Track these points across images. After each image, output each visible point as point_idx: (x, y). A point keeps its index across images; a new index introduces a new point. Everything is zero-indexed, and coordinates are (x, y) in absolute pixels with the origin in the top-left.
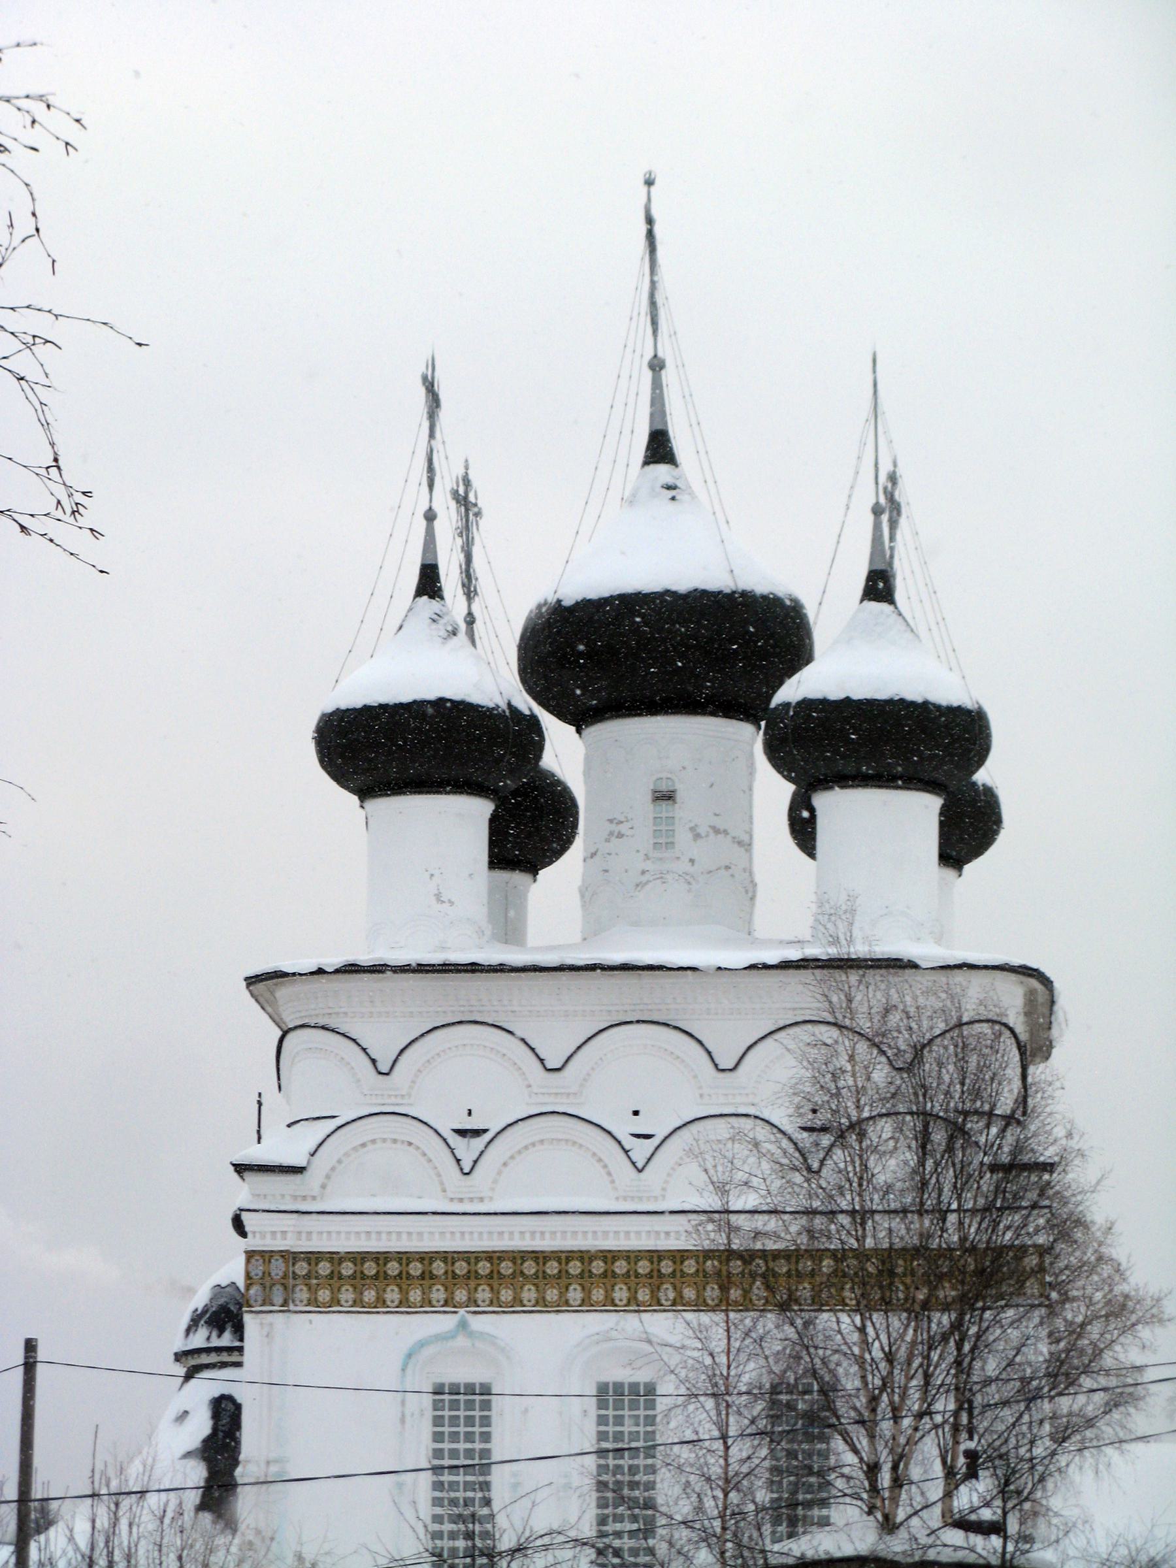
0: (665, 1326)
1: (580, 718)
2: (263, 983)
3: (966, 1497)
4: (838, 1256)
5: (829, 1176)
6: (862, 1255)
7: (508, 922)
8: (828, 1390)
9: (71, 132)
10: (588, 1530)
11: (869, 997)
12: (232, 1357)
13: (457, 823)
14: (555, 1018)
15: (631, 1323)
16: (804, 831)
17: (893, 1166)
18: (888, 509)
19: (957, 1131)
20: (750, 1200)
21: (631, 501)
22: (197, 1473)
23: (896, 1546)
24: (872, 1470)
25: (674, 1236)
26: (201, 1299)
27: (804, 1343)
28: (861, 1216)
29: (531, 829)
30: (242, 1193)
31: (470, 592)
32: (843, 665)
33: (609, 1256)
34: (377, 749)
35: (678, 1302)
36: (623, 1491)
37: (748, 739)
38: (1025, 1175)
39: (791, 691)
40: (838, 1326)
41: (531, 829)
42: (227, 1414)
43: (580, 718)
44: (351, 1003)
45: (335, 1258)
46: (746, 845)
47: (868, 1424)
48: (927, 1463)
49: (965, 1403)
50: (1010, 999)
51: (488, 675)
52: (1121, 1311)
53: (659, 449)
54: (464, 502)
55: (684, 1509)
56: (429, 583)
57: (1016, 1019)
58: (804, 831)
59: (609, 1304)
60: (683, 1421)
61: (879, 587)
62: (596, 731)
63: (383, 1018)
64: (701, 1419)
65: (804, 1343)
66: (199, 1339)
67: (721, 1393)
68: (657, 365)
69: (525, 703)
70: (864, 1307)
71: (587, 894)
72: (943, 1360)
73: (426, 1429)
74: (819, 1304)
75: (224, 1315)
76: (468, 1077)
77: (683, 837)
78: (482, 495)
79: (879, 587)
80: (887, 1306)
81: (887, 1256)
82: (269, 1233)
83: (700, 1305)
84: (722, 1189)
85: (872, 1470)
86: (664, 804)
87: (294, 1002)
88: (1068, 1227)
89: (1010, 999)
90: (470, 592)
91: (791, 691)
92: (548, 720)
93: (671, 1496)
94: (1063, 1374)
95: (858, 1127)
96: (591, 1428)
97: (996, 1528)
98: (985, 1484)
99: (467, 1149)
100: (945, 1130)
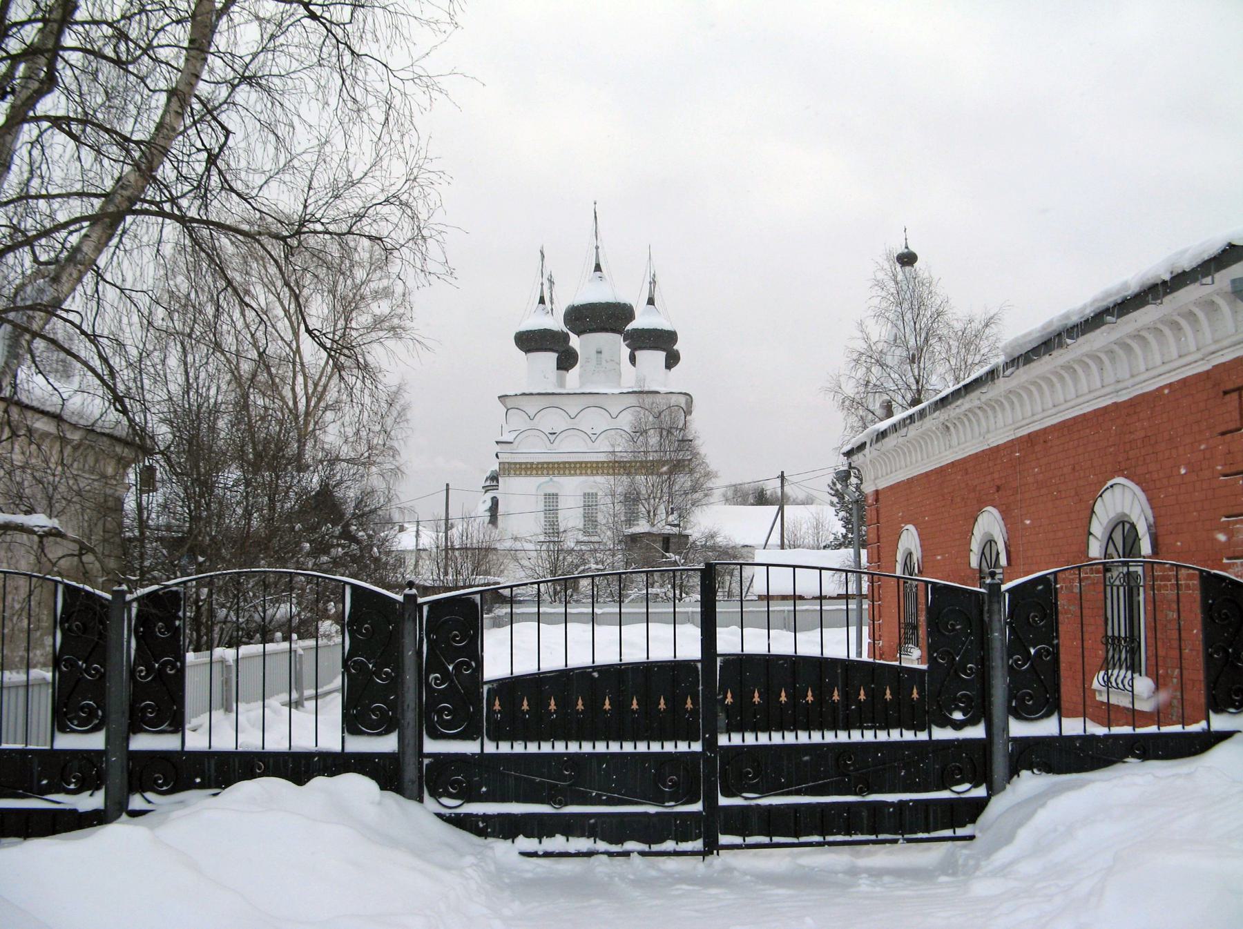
0: (600, 479)
1: (579, 333)
2: (502, 398)
3: (671, 518)
4: (641, 462)
6: (647, 462)
7: (561, 383)
9: (449, 180)
10: (581, 526)
11: (648, 400)
12: (496, 488)
13: (549, 359)
14: (573, 406)
15: (592, 478)
16: (633, 359)
17: (654, 439)
18: (653, 282)
19: (669, 432)
20: (620, 449)
23: (654, 530)
24: (649, 512)
25: (602, 458)
26: (488, 474)
27: (633, 482)
28: (646, 452)
29: (567, 360)
30: (498, 448)
31: (552, 303)
32: (642, 320)
33: (586, 463)
34: (530, 341)
35: (603, 474)
36: (590, 521)
37: (618, 338)
38: (685, 443)
39: (630, 327)
40: (640, 479)
42: (495, 502)
44: (526, 404)
45: (520, 464)
47: (647, 500)
49: (670, 495)
50: (682, 401)
51: (556, 323)
52: (708, 475)
53: (598, 268)
54: (551, 282)
55: (604, 522)
56: (542, 301)
57: (683, 405)
58: (633, 359)
59: (586, 474)
60: (605, 503)
61: (651, 301)
62: (583, 336)
63: (531, 406)
64: (609, 500)
65: (633, 482)
66: (488, 483)
68: (597, 248)
69: (565, 330)
71: (581, 376)
73: (543, 504)
75: (494, 478)
76: (552, 420)
77: (604, 362)
78: (555, 279)
79: (651, 301)
80: (652, 474)
82: (505, 458)
83: (608, 474)
84: (613, 446)
85: (649, 512)
87: (510, 402)
88: (695, 455)
89: (682, 401)
90: (552, 303)
91: (630, 327)
92: (571, 334)
93: (601, 518)
94: (694, 489)
95: (646, 431)
97: (678, 525)
98: (676, 514)
100: (667, 431)
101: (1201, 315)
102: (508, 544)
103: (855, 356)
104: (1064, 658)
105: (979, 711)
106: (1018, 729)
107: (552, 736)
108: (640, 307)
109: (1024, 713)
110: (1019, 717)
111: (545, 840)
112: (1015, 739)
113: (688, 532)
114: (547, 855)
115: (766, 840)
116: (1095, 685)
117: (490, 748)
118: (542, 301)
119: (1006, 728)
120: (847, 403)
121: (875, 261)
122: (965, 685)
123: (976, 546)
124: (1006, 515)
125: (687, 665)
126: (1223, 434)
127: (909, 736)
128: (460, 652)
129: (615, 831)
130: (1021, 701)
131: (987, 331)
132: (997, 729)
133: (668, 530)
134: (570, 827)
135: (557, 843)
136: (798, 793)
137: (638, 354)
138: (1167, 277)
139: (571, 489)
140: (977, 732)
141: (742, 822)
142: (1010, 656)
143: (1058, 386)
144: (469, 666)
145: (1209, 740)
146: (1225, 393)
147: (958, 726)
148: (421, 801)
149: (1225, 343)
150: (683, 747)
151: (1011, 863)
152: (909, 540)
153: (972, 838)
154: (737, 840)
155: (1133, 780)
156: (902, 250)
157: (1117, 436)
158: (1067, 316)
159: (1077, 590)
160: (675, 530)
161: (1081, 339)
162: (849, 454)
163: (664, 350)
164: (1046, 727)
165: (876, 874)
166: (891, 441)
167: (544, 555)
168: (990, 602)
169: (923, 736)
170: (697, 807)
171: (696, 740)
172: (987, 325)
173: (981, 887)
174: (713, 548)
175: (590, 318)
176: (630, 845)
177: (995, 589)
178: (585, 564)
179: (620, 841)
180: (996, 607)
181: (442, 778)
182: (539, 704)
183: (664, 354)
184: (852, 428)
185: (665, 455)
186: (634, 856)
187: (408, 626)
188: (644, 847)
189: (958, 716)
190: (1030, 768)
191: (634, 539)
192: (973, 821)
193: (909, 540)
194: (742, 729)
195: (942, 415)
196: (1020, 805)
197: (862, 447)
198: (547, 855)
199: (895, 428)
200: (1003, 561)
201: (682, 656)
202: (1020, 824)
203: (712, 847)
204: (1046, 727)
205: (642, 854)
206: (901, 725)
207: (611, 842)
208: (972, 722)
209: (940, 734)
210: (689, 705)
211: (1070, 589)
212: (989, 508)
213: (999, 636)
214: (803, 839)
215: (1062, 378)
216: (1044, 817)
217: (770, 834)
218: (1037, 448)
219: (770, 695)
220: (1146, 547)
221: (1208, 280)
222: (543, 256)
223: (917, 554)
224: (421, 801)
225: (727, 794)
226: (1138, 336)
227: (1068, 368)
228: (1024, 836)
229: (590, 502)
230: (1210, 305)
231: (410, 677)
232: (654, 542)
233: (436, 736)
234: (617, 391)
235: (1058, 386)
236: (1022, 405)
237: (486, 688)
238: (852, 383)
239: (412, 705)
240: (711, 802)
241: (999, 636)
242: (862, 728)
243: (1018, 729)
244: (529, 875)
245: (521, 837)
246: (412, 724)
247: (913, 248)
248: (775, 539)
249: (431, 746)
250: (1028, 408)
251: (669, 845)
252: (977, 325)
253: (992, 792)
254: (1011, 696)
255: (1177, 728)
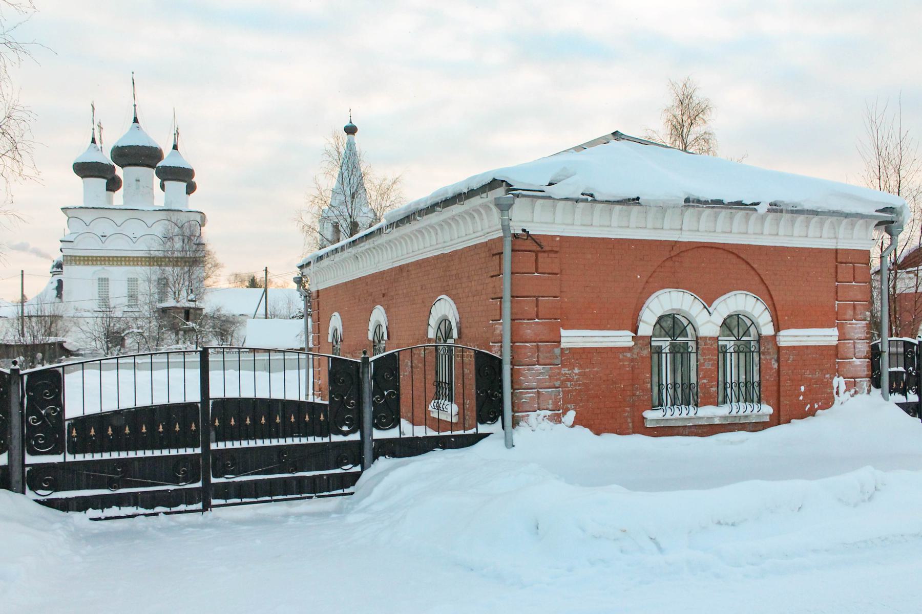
5: (167, 246)
7: (110, 200)
8: (167, 280)
11: (174, 217)
14: (119, 217)
16: (163, 187)
17: (178, 245)
18: (177, 134)
19: (189, 239)
21: (510, 444)
22: (56, 292)
23: (178, 305)
27: (163, 272)
29: (113, 184)
34: (85, 170)
36: (132, 296)
39: (160, 164)
40: (169, 269)
41: (113, 184)
42: (60, 282)
43: (122, 167)
46: (152, 189)
48: (184, 293)
49: (190, 281)
51: (106, 158)
53: (136, 120)
56: (93, 141)
57: (199, 220)
60: (143, 287)
61: (175, 147)
63: (88, 216)
66: (55, 269)
67: (149, 281)
68: (135, 106)
69: (113, 163)
70: (174, 266)
71: (124, 196)
72: (187, 276)
73: (97, 288)
74: (166, 265)
75: (59, 266)
79: (175, 147)
80: (177, 266)
81: (177, 258)
86: (103, 276)
89: (198, 217)
91: (160, 164)
92: (116, 166)
96: (126, 291)
99: (104, 239)
101: (483, 212)
102: (71, 313)
103: (311, 198)
104: (402, 397)
105: (357, 425)
106: (378, 434)
107: (110, 450)
108: (167, 151)
109: (379, 426)
110: (378, 428)
111: (105, 510)
112: (376, 440)
113: (201, 305)
114: (107, 518)
115: (238, 501)
116: (430, 408)
117: (70, 458)
118: (93, 141)
119: (371, 434)
120: (306, 228)
121: (326, 140)
122: (349, 411)
123: (371, 327)
124: (387, 311)
125: (192, 405)
126: (492, 277)
127: (319, 440)
128: (49, 403)
129: (150, 501)
130: (380, 420)
131: (395, 186)
132: (366, 435)
133: (188, 305)
134: (120, 501)
135: (114, 511)
136: (252, 474)
137: (166, 183)
138: (466, 191)
139: (118, 275)
140: (356, 437)
141: (225, 492)
142: (374, 396)
143: (415, 241)
144: (55, 410)
145: (478, 438)
146: (494, 255)
147: (345, 434)
148: (24, 493)
149: (494, 229)
150: (190, 451)
151: (367, 507)
152: (336, 322)
153: (352, 494)
154: (222, 502)
155: (437, 458)
156: (347, 123)
157: (444, 272)
158: (418, 203)
159: (422, 355)
160: (192, 305)
161: (425, 217)
162: (301, 267)
163: (184, 181)
164: (393, 434)
165: (298, 516)
166: (325, 262)
167: (100, 323)
168: (363, 368)
169: (326, 440)
170: (199, 485)
171: (198, 447)
172: (394, 183)
173: (352, 518)
174: (219, 318)
175: (131, 155)
176: (158, 509)
177: (365, 360)
178: (129, 328)
179: (153, 507)
180: (366, 370)
181: (36, 479)
182: (101, 431)
183: (185, 184)
184: (309, 244)
185: (187, 255)
186: (161, 515)
187: (13, 388)
188: (168, 510)
189: (345, 428)
190: (384, 455)
191: (165, 311)
192: (354, 485)
193: (336, 322)
194: (224, 440)
195: (353, 251)
196: (378, 474)
197: (309, 264)
198: (107, 518)
199: (327, 254)
200: (385, 337)
201: (189, 400)
202: (376, 485)
203: (207, 507)
204: (393, 434)
205: (166, 513)
206: (313, 434)
207: (147, 508)
208: (353, 431)
209: (336, 438)
210: (193, 427)
211: (419, 355)
212: (378, 306)
213: (368, 385)
214: (260, 499)
215: (416, 236)
216: (388, 480)
217: (240, 497)
218: (404, 274)
219: (240, 420)
220: (455, 335)
221: (484, 195)
222: (94, 109)
223: (340, 330)
224: (24, 493)
225: (215, 476)
226: (453, 218)
227: (419, 231)
228: (377, 491)
229: (132, 281)
230: (486, 207)
231: (16, 420)
232: (178, 313)
233: (33, 453)
234: (152, 209)
235: (415, 241)
236: (397, 250)
237: (67, 423)
238: (310, 215)
239: (17, 436)
240: (206, 481)
241: (368, 385)
242: (292, 436)
243: (378, 434)
244: (96, 531)
245: (90, 509)
246: (17, 447)
247: (354, 123)
248: (262, 311)
249: (30, 460)
250: (400, 252)
251: (182, 507)
252: (388, 182)
253: (363, 469)
254: (375, 416)
255: (461, 432)
